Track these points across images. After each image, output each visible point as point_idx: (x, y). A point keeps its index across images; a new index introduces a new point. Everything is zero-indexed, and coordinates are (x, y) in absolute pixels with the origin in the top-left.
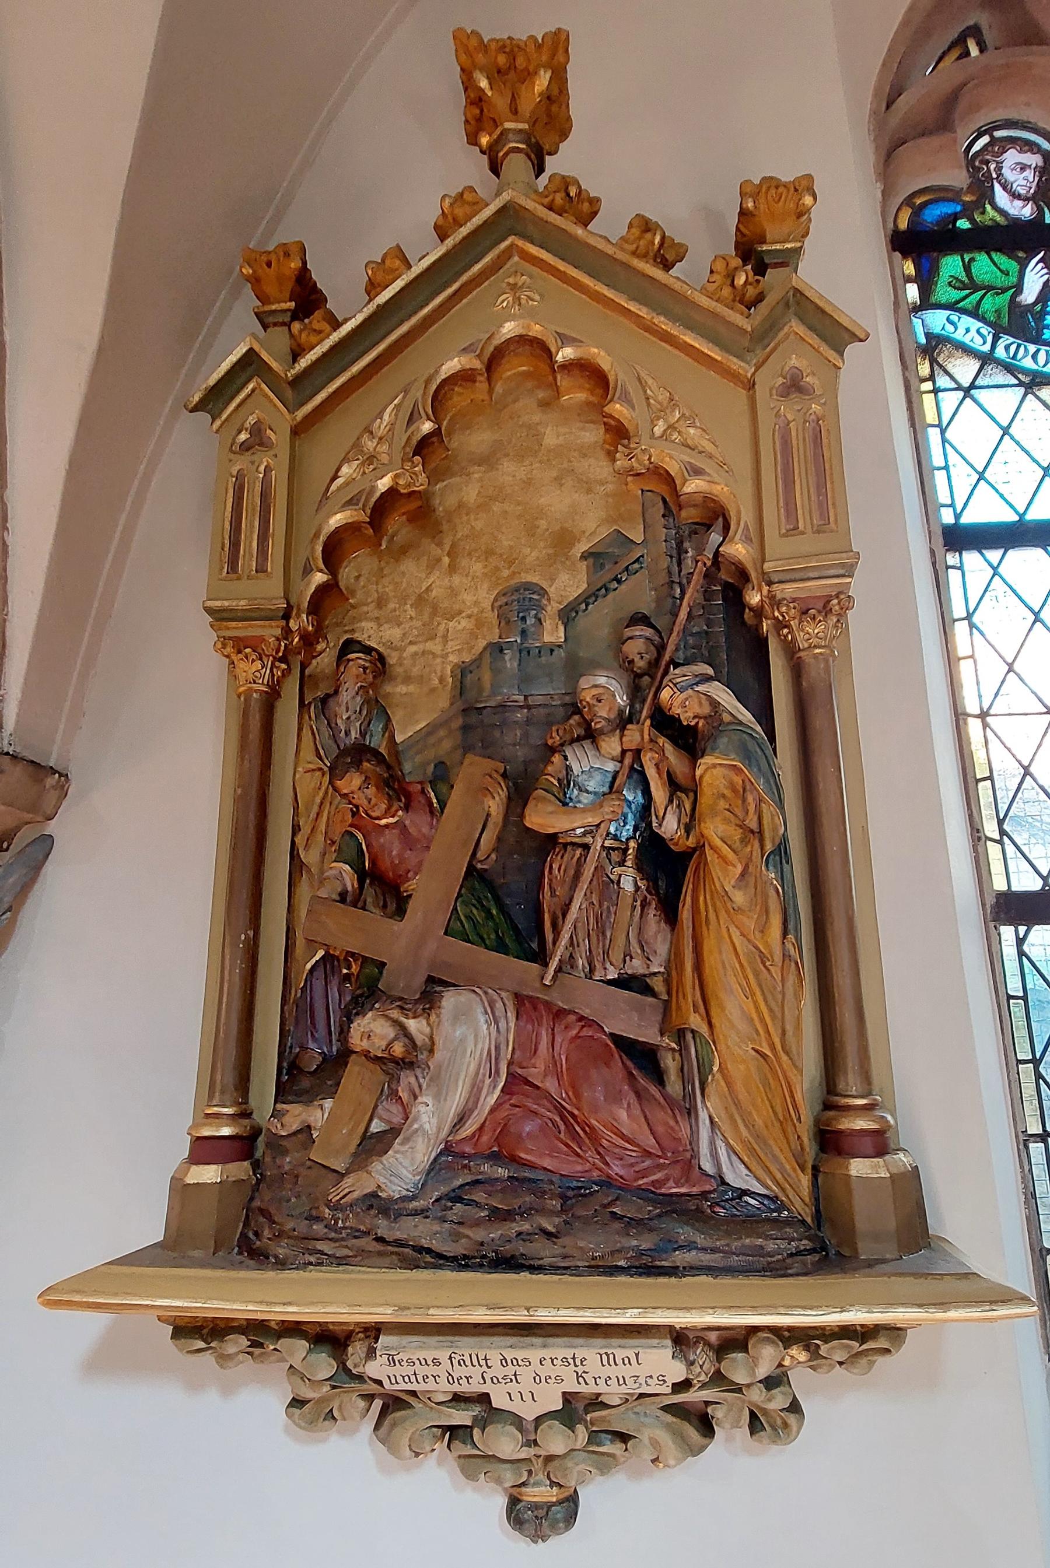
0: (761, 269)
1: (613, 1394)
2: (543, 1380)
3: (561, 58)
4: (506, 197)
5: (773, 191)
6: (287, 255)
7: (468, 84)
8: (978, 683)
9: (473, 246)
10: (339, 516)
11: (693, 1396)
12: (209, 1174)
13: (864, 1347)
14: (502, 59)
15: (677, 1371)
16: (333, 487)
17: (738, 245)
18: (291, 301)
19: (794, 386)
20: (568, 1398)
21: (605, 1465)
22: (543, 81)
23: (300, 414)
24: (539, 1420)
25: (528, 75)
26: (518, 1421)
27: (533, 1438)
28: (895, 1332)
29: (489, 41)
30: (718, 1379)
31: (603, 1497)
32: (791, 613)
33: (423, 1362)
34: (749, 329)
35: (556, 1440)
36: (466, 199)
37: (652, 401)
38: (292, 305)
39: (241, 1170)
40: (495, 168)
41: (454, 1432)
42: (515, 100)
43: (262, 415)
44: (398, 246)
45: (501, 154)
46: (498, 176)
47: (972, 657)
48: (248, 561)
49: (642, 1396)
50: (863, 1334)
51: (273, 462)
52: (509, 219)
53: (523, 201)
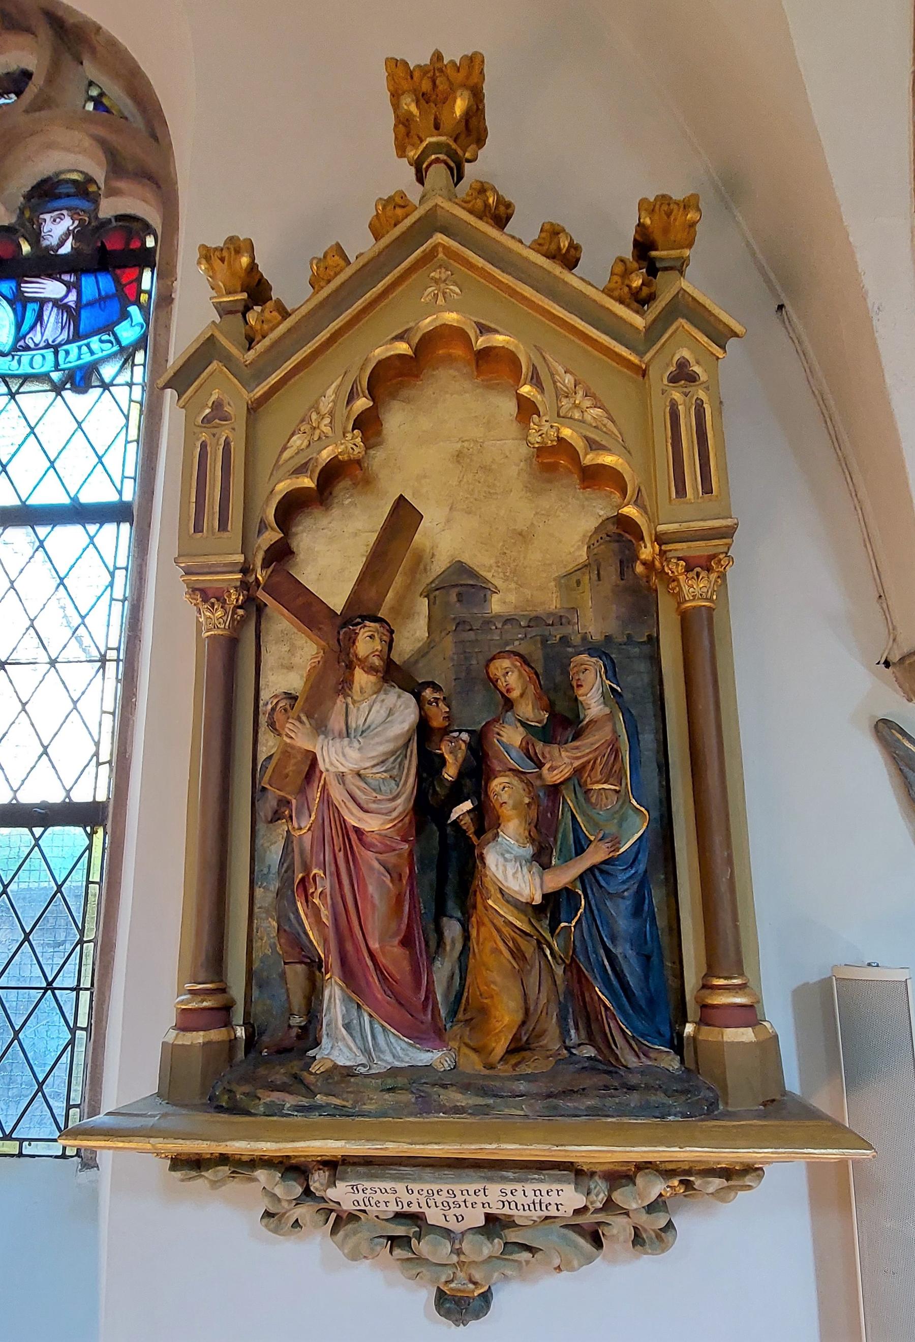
0: (653, 270)
1: (518, 1215)
2: (435, 1193)
5: (665, 207)
6: (238, 252)
7: (396, 106)
9: (406, 242)
13: (731, 1183)
14: (426, 86)
15: (580, 1201)
17: (636, 243)
18: (242, 291)
19: (683, 375)
20: (489, 1217)
22: (460, 106)
23: (260, 391)
25: (447, 99)
26: (447, 1233)
27: (457, 1246)
28: (750, 1170)
31: (507, 1298)
33: (383, 1191)
36: (396, 203)
37: (558, 384)
39: (217, 1035)
40: (420, 179)
41: (394, 1241)
42: (442, 112)
44: (338, 245)
45: (424, 166)
46: (423, 184)
47: (127, 442)
49: (547, 1218)
50: (727, 1173)
51: (233, 432)
52: (431, 223)
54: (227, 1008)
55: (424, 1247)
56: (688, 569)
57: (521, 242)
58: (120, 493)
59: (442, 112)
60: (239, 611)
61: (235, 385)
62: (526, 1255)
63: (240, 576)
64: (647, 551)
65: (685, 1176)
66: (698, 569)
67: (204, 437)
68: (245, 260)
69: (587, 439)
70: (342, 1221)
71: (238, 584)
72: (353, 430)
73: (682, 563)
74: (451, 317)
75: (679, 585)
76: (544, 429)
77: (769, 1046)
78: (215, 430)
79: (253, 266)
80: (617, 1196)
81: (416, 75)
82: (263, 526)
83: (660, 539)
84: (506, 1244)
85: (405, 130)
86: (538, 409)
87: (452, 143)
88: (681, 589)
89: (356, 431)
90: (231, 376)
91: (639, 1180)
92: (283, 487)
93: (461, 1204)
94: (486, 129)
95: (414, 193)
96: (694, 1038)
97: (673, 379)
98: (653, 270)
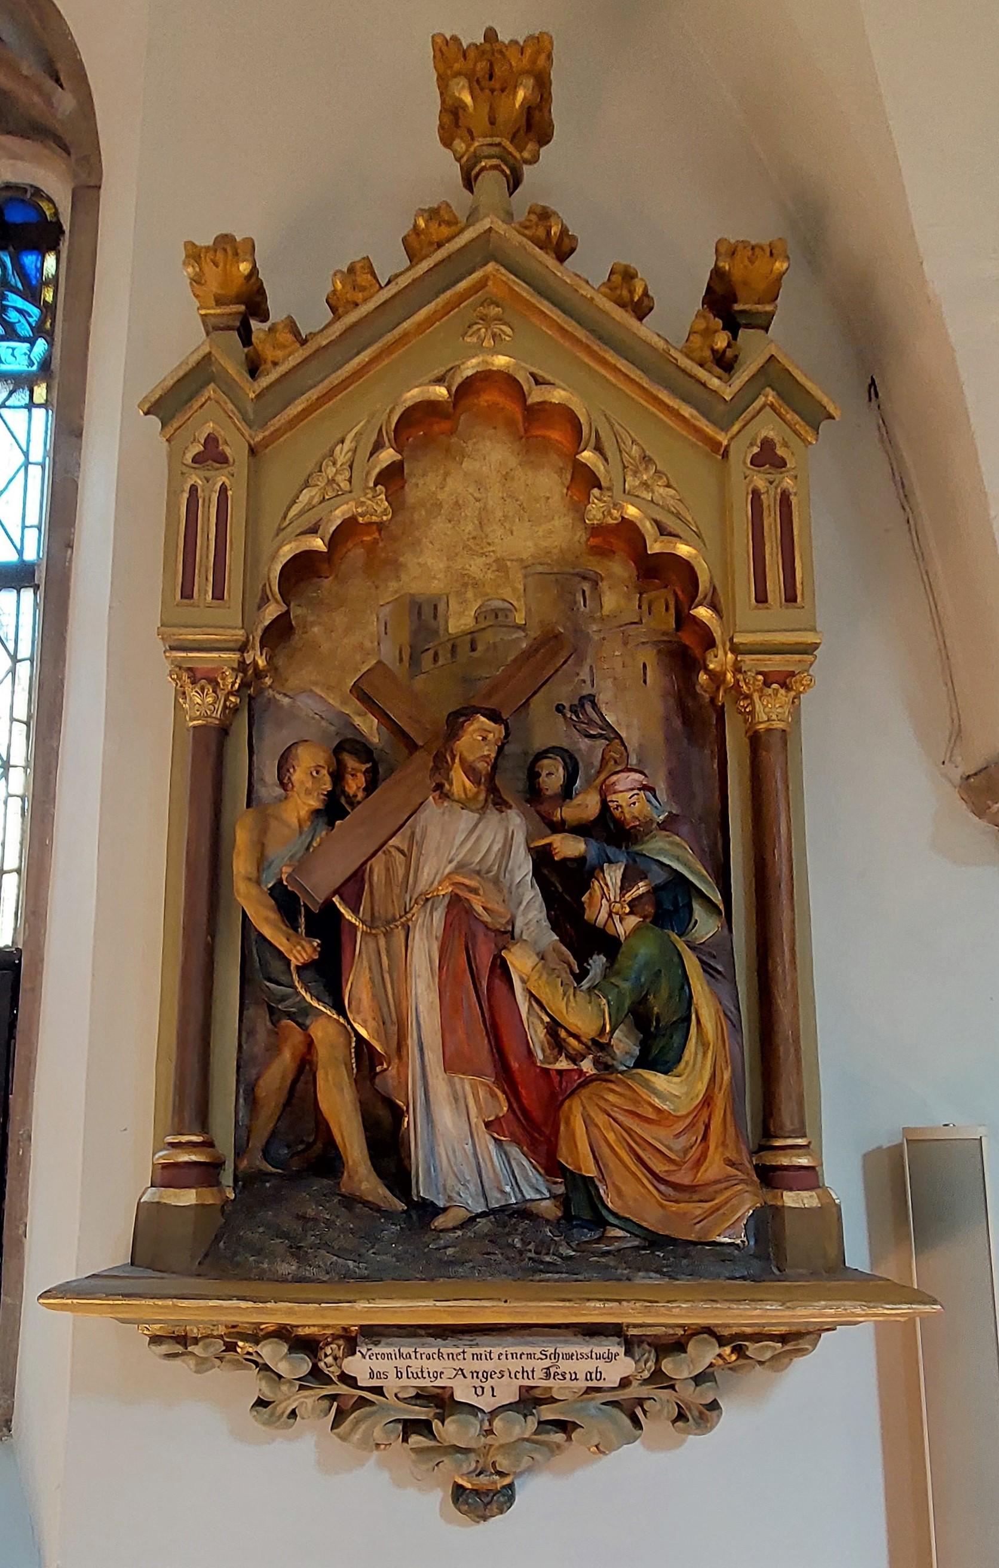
3: (541, 61)
4: (486, 224)
8: (5, 829)
9: (444, 261)
13: (787, 1348)
16: (292, 513)
19: (767, 457)
24: (494, 1413)
25: (508, 88)
26: (473, 1410)
29: (469, 46)
30: (658, 1378)
31: (534, 1492)
39: (210, 1197)
40: (469, 183)
46: (472, 192)
48: (204, 587)
52: (486, 249)
53: (501, 227)
55: (450, 1430)
56: (767, 684)
58: (20, 552)
59: (500, 106)
60: (232, 699)
61: (749, 588)
62: (559, 1437)
64: (719, 660)
65: (738, 1342)
67: (195, 479)
68: (244, 267)
69: (657, 523)
70: (348, 1406)
71: (236, 666)
72: (375, 485)
73: (760, 677)
74: (501, 361)
75: (752, 703)
77: (829, 1216)
78: (208, 474)
79: (254, 271)
80: (668, 1366)
81: (472, 54)
82: (265, 600)
84: (540, 1423)
85: (452, 122)
86: (598, 479)
87: (506, 143)
88: (754, 708)
89: (379, 487)
91: (690, 1348)
92: (288, 551)
94: (551, 125)
95: (459, 200)
98: (732, 325)
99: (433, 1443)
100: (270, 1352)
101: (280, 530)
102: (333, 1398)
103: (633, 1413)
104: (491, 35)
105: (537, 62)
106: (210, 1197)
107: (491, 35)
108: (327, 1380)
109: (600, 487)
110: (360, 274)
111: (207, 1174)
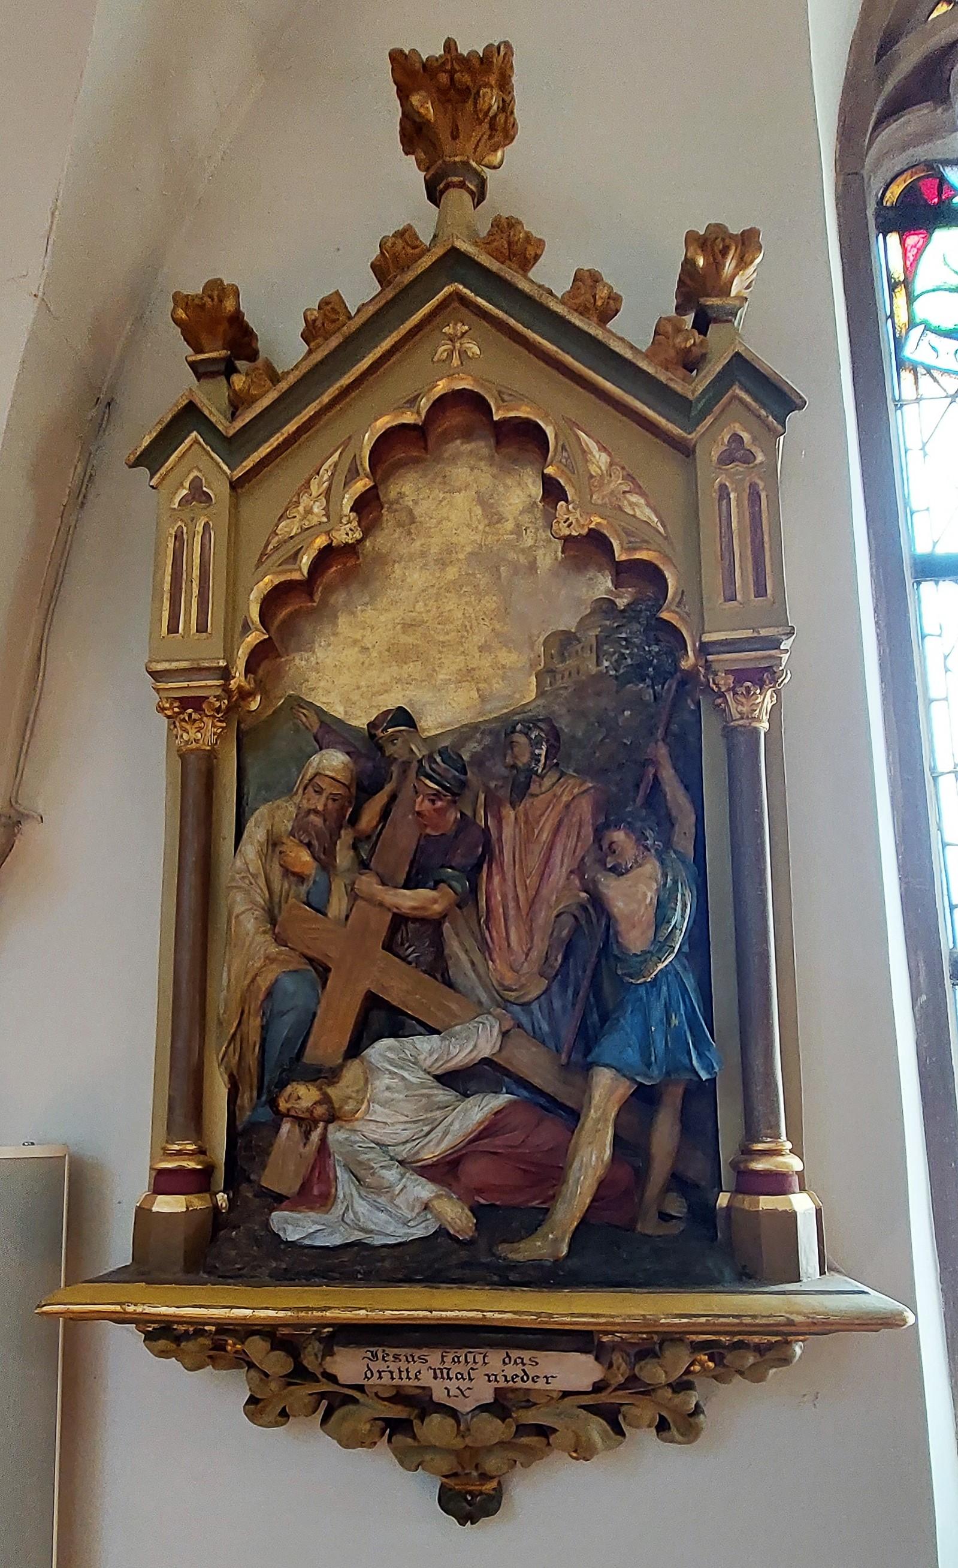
9: (419, 282)
10: (386, 419)
11: (603, 1398)
12: (169, 1204)
21: (532, 1456)
26: (453, 1413)
30: (633, 1380)
32: (724, 681)
34: (685, 665)
35: (492, 1429)
38: (223, 353)
39: (199, 1203)
41: (394, 1427)
42: (451, 105)
43: (199, 474)
46: (438, 206)
54: (208, 1171)
57: (551, 293)
63: (222, 682)
66: (749, 684)
70: (334, 1404)
76: (573, 519)
82: (246, 628)
83: (704, 649)
90: (167, 596)
93: (467, 1382)
96: (729, 1208)
97: (727, 458)
99: (416, 1444)
100: (256, 1348)
101: (260, 562)
102: (323, 1395)
103: (614, 1420)
104: (450, 45)
105: (492, 67)
106: (199, 1203)
107: (450, 45)
108: (312, 1377)
109: (567, 501)
110: (332, 306)
111: (196, 1182)
